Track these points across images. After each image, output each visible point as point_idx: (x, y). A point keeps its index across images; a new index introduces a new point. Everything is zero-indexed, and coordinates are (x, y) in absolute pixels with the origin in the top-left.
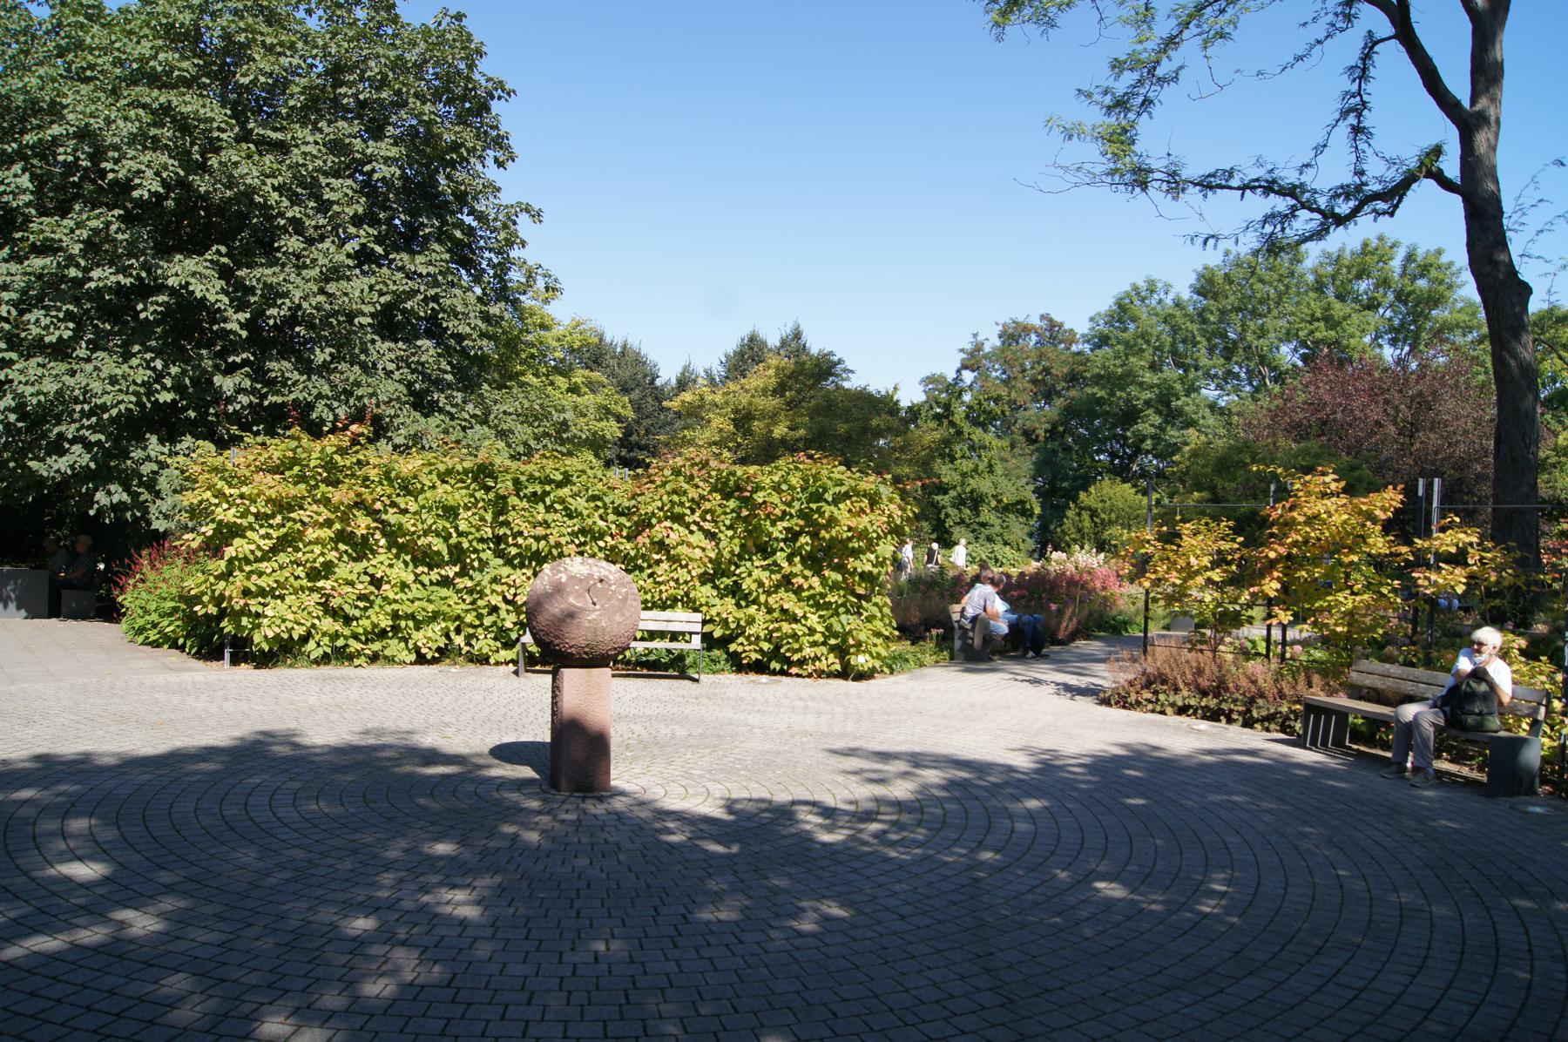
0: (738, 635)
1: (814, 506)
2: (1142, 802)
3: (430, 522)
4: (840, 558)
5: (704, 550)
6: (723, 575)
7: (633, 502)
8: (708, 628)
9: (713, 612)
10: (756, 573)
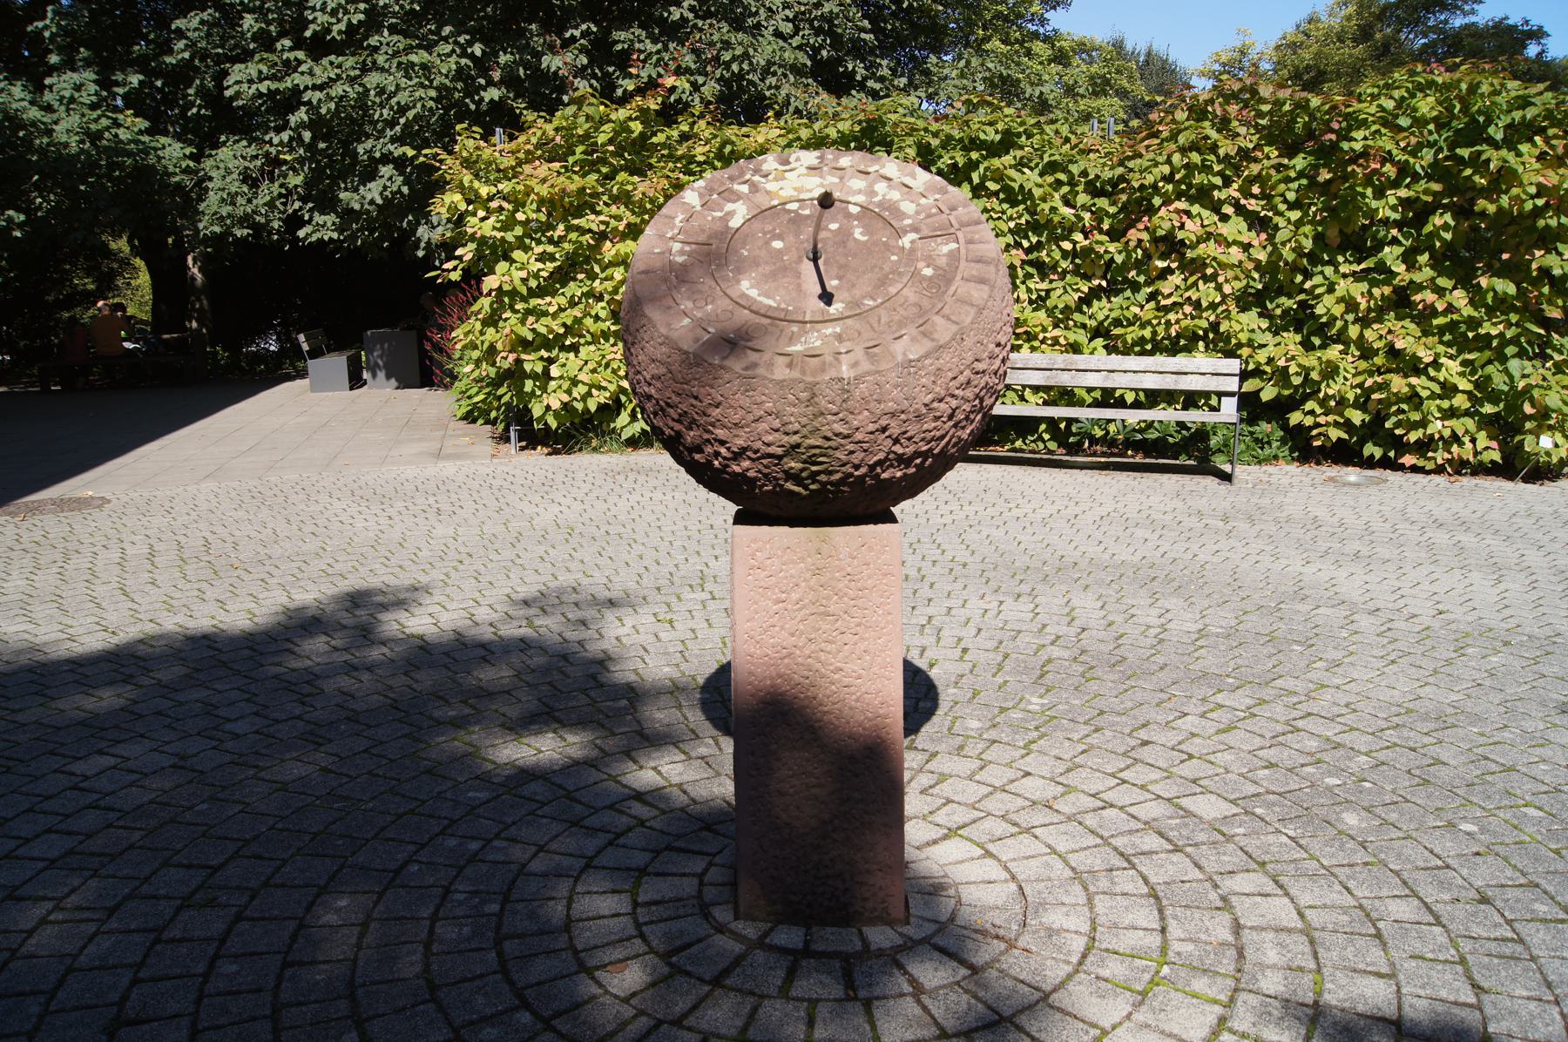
0: (1306, 398)
1: (1465, 152)
4: (1515, 250)
5: (1246, 247)
6: (1281, 292)
7: (1120, 170)
8: (1250, 385)
9: (1262, 357)
10: (1342, 287)
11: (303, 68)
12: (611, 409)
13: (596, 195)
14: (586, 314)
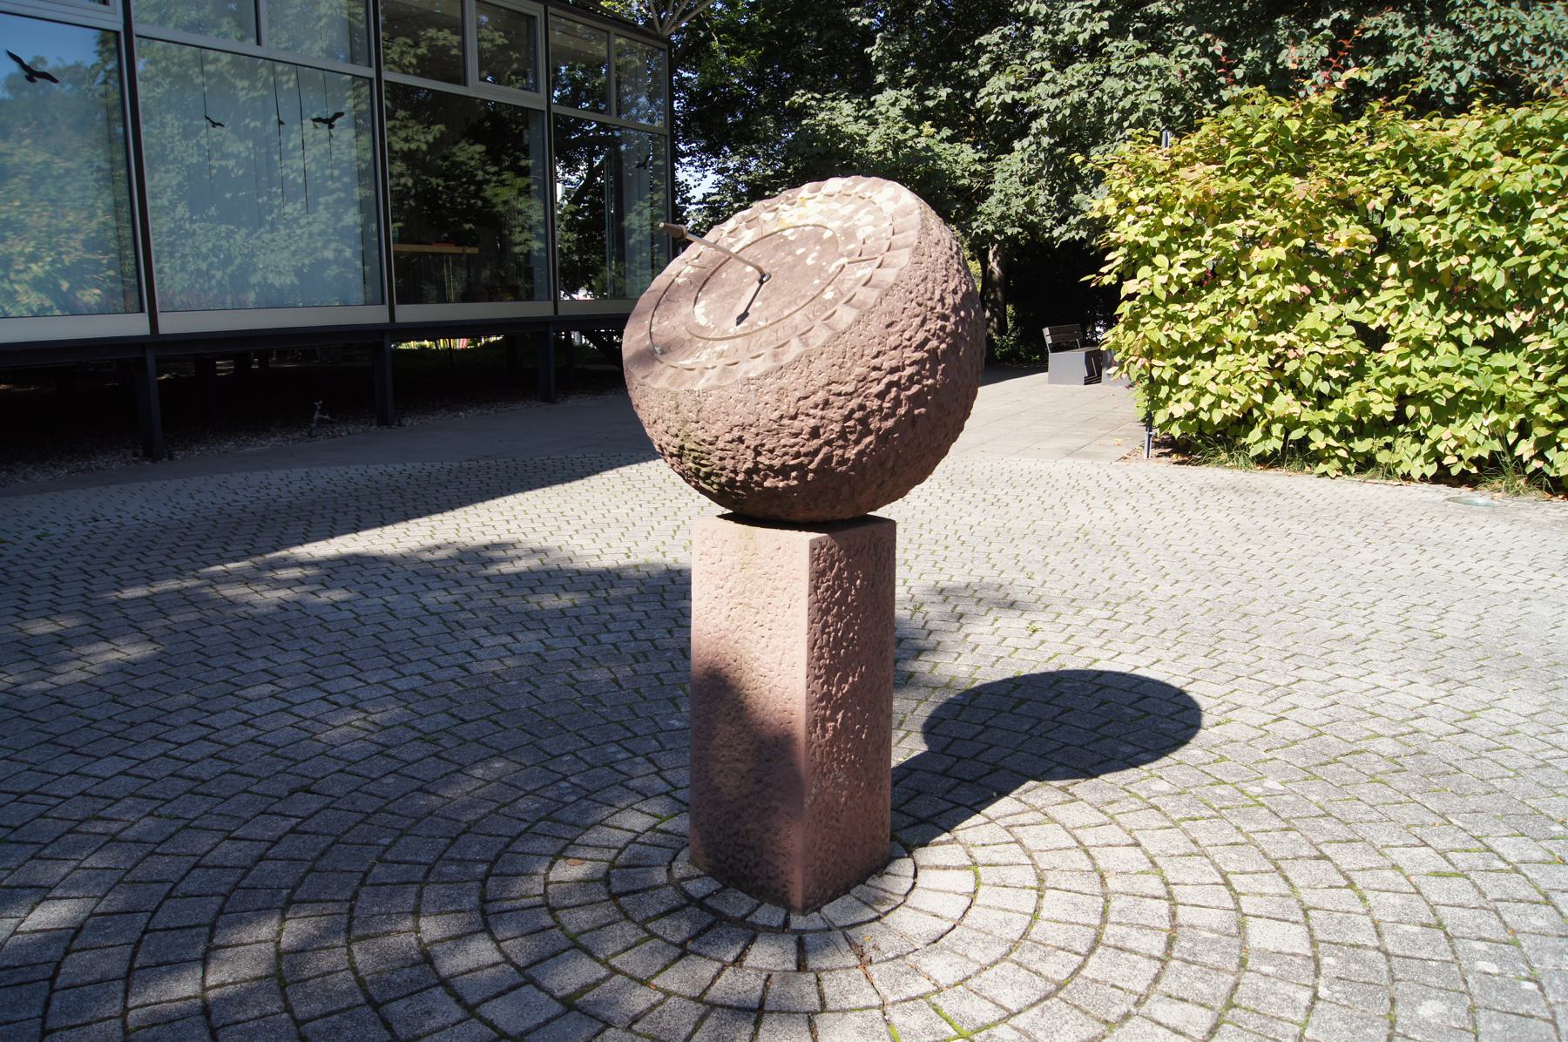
2: (404, 346)
3: (1462, 226)
11: (1047, 77)
12: (1244, 422)
13: (1251, 198)
14: (1226, 322)
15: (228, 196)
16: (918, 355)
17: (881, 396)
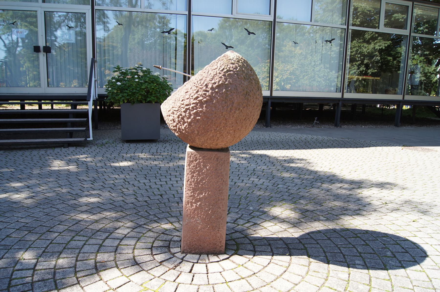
15: (332, 62)
16: (195, 101)
17: (185, 112)
